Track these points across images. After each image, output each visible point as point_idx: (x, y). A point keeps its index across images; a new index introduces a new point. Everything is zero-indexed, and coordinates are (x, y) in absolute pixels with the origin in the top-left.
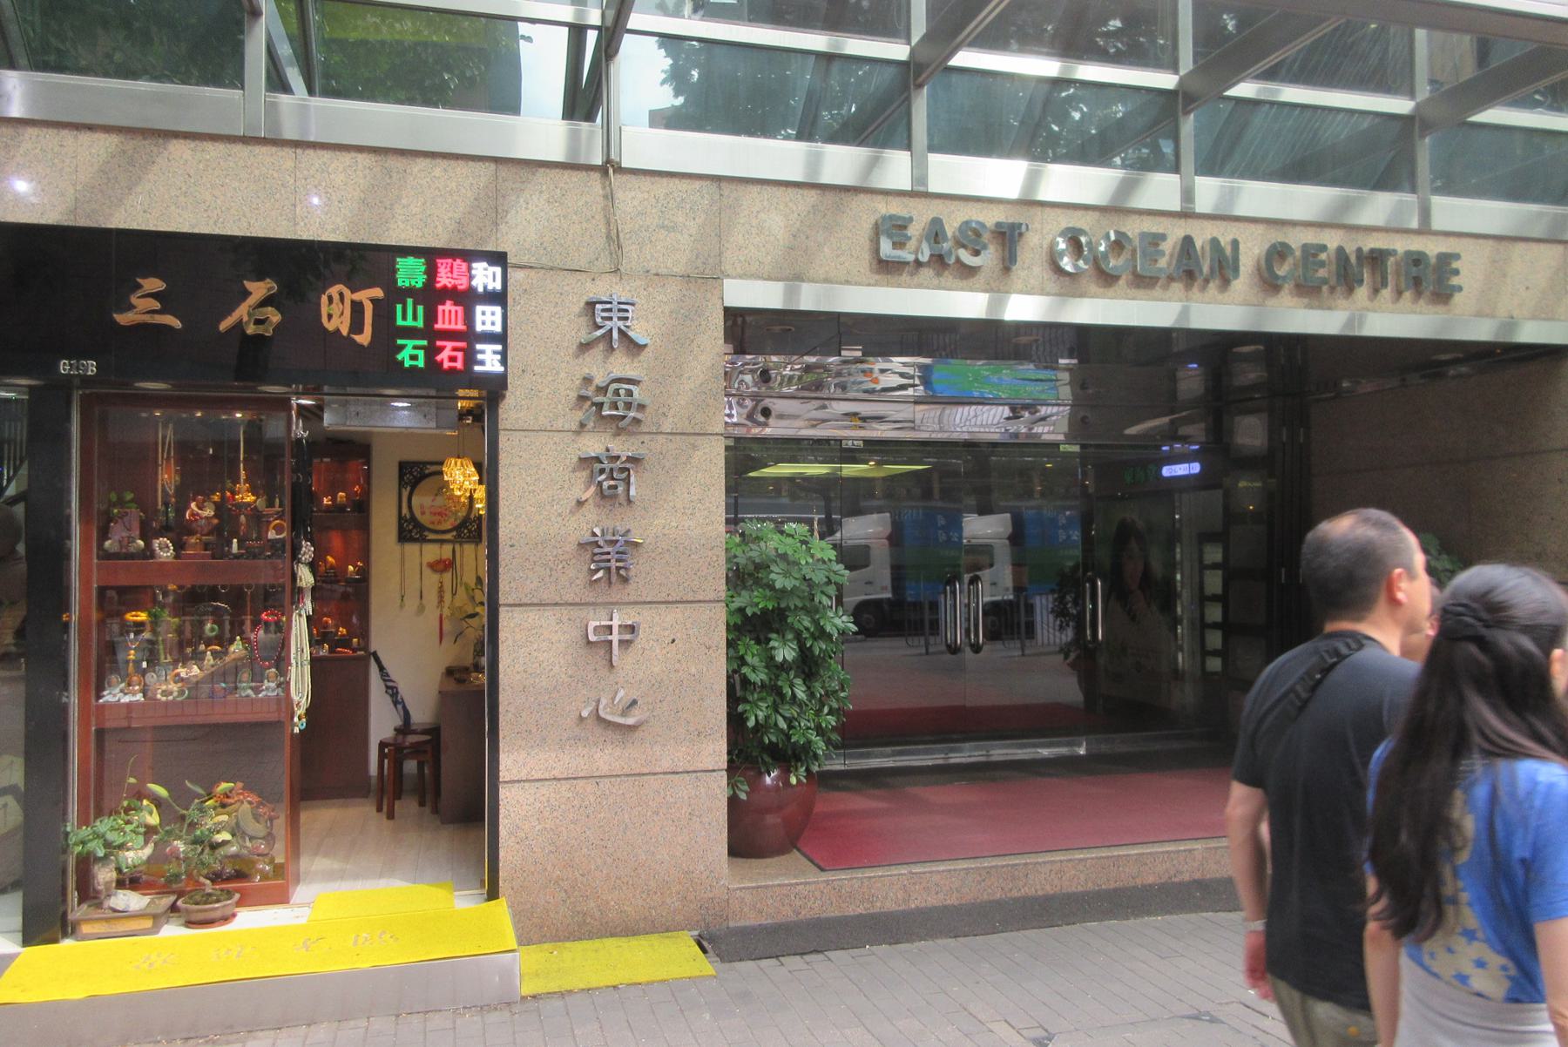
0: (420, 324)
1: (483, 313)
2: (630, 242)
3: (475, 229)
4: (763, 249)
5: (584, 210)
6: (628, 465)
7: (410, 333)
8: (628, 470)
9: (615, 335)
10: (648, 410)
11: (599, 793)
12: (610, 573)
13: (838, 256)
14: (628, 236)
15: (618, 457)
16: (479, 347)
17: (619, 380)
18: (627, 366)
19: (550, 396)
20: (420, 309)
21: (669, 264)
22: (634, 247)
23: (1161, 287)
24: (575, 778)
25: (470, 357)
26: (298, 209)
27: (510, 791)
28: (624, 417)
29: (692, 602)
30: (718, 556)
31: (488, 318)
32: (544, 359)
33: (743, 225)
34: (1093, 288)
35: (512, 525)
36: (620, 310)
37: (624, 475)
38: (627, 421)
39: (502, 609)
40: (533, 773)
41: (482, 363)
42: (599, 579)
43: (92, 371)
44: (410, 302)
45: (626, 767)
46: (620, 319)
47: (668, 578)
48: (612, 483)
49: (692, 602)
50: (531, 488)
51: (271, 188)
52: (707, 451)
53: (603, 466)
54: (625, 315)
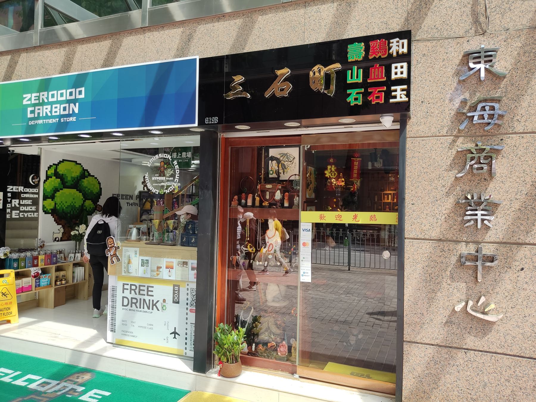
0: (360, 80)
1: (396, 68)
2: (495, 13)
3: (396, 25)
7: (355, 86)
8: (491, 157)
10: (505, 118)
11: (466, 359)
12: (477, 222)
16: (393, 88)
17: (485, 100)
19: (439, 115)
20: (361, 71)
22: (498, 16)
23: (304, 210)
24: (450, 347)
25: (389, 95)
26: (306, 33)
27: (410, 347)
31: (399, 70)
32: (435, 93)
35: (413, 192)
36: (486, 57)
39: (406, 241)
40: (424, 339)
41: (395, 97)
42: (470, 226)
43: (216, 121)
44: (355, 68)
45: (486, 346)
48: (479, 166)
50: (425, 170)
51: (294, 26)
53: (473, 155)
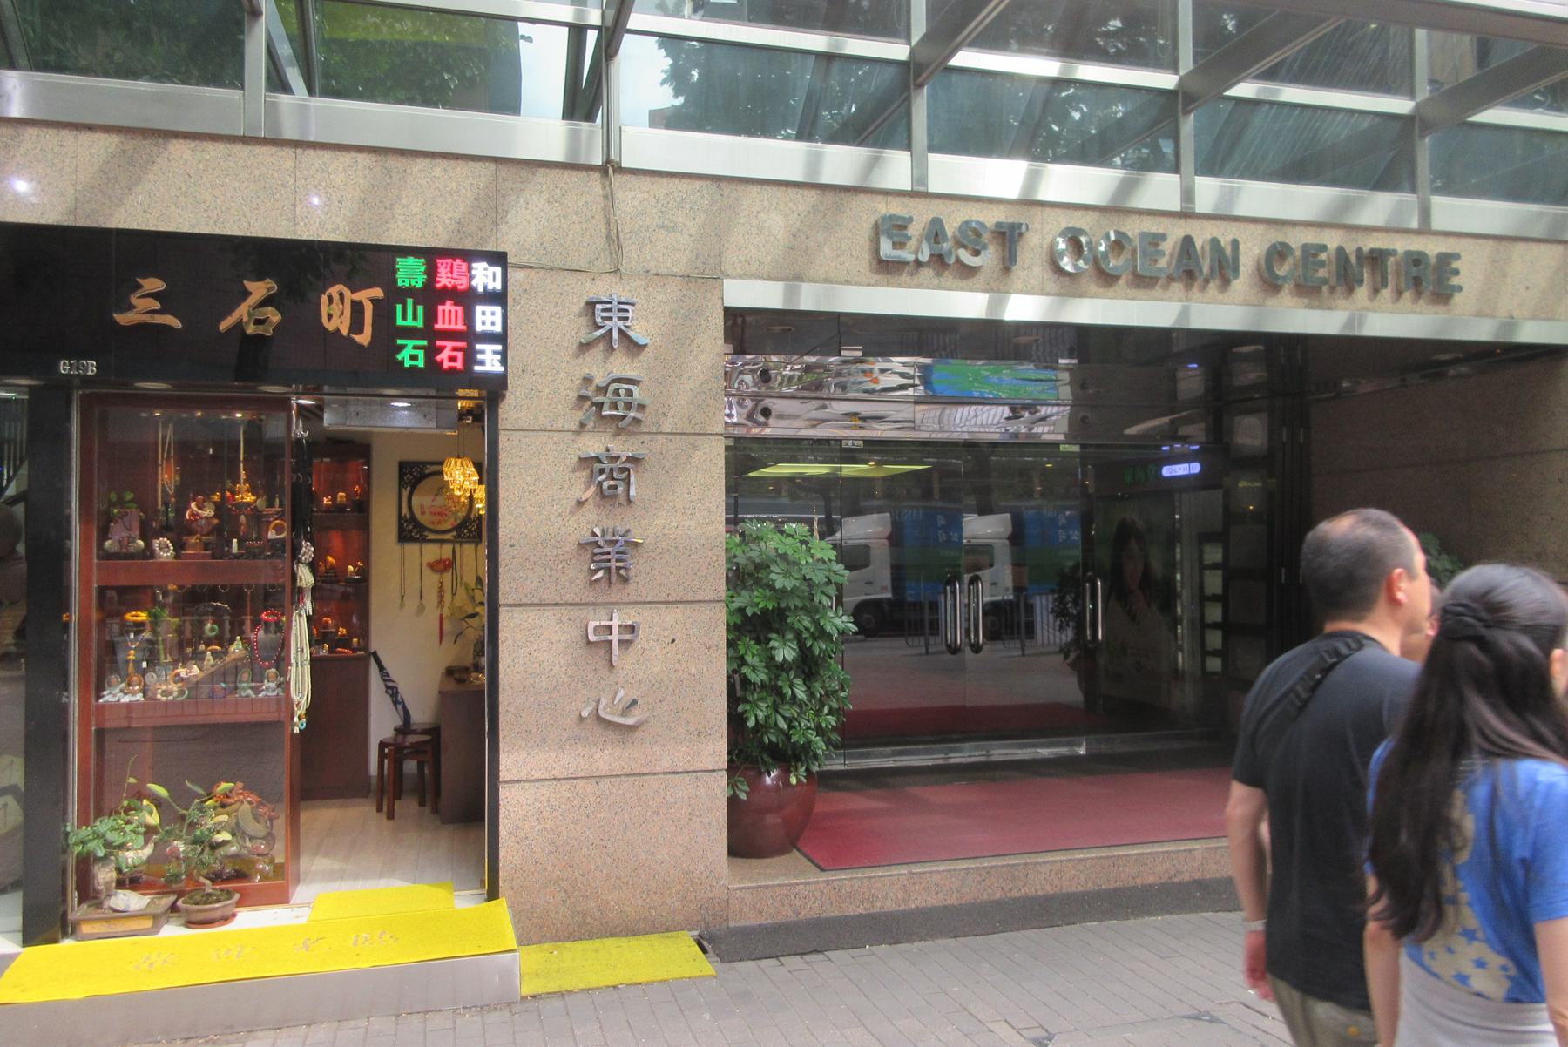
0: (420, 324)
1: (483, 313)
2: (630, 242)
3: (475, 229)
4: (763, 249)
5: (584, 210)
6: (628, 465)
7: (410, 333)
8: (628, 470)
9: (615, 335)
10: (648, 410)
11: (599, 793)
12: (610, 573)
13: (838, 256)
14: (628, 236)
15: (618, 457)
16: (479, 347)
17: (619, 380)
18: (627, 366)
19: (550, 396)
20: (420, 309)
21: (669, 264)
22: (634, 247)
23: (1161, 287)
24: (575, 778)
25: (470, 357)
26: (298, 209)
27: (510, 791)
28: (624, 417)
29: (692, 602)
30: (718, 556)
31: (488, 318)
32: (544, 359)
33: (743, 225)
34: (1093, 288)
35: (512, 525)
36: (620, 310)
37: (624, 475)
38: (627, 421)
39: (502, 609)
40: (533, 773)
41: (482, 363)
42: (599, 579)
43: (92, 371)
44: (410, 302)
45: (626, 767)
46: (620, 319)
47: (668, 578)
48: (612, 483)
49: (692, 602)
50: (531, 488)
51: (271, 188)
52: (707, 451)
53: (603, 466)
54: (625, 315)
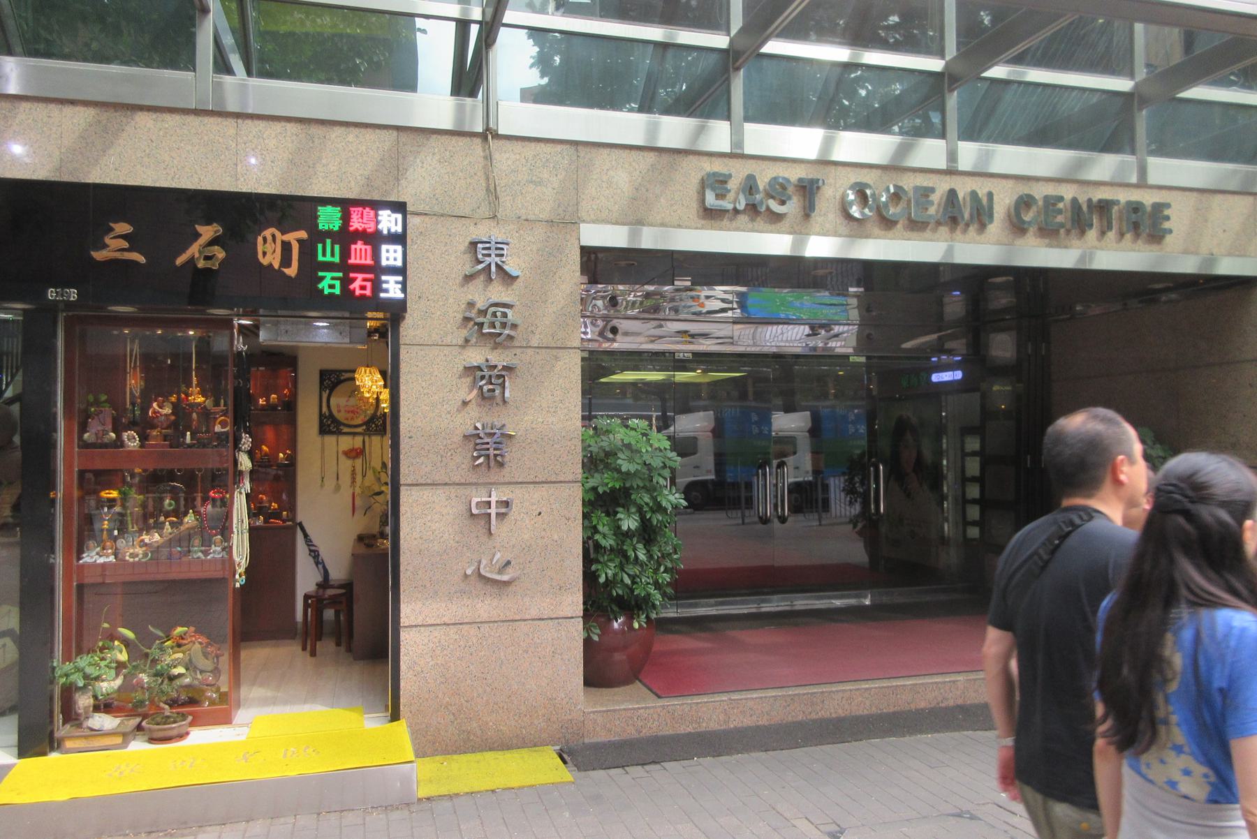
0: (337, 259)
1: (388, 251)
2: (505, 194)
3: (381, 183)
4: (612, 200)
5: (469, 168)
6: (503, 373)
7: (329, 267)
8: (504, 377)
9: (493, 268)
10: (520, 329)
11: (480, 636)
12: (489, 459)
13: (672, 205)
14: (503, 189)
15: (495, 367)
16: (384, 278)
17: (496, 305)
18: (503, 294)
19: (441, 317)
20: (337, 248)
21: (537, 212)
22: (508, 198)
23: (930, 230)
24: (461, 624)
25: (377, 286)
26: (239, 168)
27: (409, 634)
28: (500, 334)
29: (554, 482)
30: (575, 446)
31: (392, 255)
32: (436, 287)
33: (596, 180)
34: (876, 231)
35: (410, 421)
36: (497, 249)
37: (500, 381)
38: (502, 337)
39: (402, 488)
40: (427, 619)
41: (386, 291)
42: (480, 464)
43: (74, 297)
44: (328, 242)
45: (502, 614)
46: (497, 255)
47: (535, 463)
48: (491, 387)
49: (554, 482)
50: (425, 391)
51: (217, 151)
52: (566, 361)
53: (483, 373)
54: (501, 252)
